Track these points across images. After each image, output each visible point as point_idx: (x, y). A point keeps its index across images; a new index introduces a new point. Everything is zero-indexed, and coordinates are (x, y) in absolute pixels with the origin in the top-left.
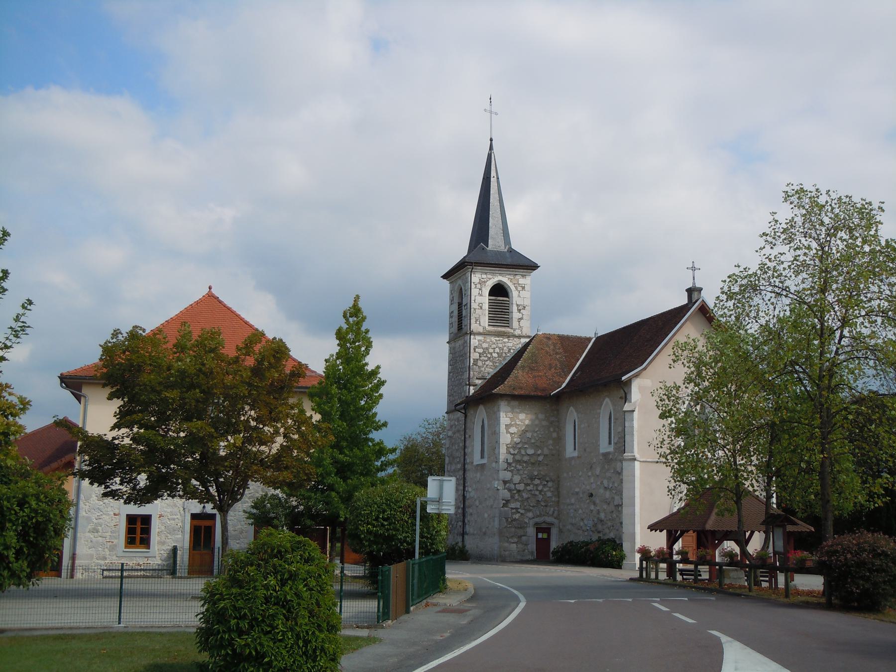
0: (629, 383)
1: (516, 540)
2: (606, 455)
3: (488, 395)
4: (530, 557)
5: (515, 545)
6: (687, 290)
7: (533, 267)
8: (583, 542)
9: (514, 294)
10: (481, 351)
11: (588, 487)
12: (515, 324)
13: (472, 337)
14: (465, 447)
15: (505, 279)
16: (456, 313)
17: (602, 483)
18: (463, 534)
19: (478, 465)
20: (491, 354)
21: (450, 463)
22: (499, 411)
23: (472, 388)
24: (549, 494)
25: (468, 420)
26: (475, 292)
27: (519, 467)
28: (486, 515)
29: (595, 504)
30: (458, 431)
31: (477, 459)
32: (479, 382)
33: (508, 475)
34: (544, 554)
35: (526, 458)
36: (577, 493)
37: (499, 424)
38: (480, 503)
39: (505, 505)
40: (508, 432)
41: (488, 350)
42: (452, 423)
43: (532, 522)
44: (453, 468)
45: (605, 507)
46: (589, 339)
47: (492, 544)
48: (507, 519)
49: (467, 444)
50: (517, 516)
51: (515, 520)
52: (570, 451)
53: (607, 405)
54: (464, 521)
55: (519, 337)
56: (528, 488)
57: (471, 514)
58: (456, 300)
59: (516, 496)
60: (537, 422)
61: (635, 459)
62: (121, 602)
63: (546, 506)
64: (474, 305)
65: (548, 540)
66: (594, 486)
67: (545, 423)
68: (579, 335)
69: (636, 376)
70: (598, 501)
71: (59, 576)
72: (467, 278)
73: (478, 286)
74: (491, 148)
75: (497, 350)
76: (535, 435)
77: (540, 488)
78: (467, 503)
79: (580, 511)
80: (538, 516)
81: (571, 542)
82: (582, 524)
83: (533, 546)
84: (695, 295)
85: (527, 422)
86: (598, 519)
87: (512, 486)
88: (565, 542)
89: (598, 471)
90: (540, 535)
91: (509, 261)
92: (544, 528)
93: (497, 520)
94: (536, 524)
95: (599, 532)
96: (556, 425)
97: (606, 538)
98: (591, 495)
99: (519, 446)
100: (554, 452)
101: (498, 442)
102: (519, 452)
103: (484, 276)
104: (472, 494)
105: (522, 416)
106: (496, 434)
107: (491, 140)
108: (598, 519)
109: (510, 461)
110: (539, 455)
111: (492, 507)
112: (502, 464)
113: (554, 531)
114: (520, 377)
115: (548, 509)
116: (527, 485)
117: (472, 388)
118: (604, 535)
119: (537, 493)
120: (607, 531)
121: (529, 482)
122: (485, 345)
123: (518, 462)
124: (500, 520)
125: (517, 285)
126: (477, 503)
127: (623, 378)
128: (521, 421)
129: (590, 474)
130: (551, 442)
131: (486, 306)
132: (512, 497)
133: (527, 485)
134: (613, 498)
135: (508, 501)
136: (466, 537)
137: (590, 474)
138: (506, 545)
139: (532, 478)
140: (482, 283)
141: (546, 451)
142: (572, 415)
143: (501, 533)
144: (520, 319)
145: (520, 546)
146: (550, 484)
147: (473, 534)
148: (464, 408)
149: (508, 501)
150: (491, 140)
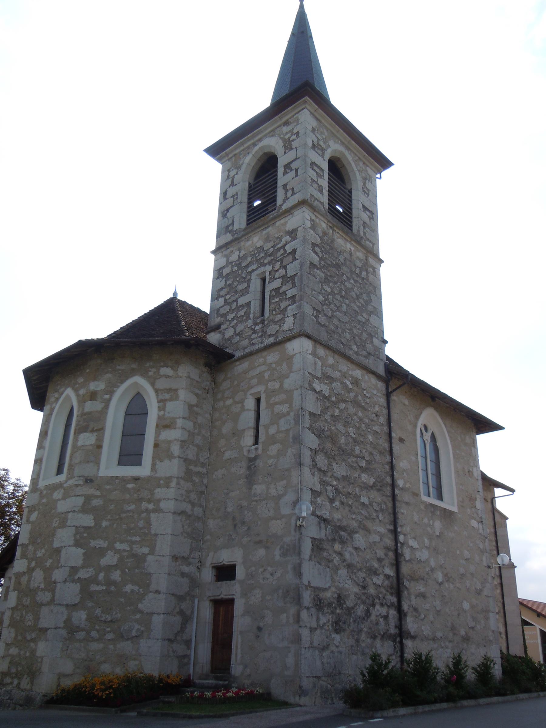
38: (448, 578)
57: (423, 596)
104: (424, 555)
111: (479, 592)
126: (440, 577)
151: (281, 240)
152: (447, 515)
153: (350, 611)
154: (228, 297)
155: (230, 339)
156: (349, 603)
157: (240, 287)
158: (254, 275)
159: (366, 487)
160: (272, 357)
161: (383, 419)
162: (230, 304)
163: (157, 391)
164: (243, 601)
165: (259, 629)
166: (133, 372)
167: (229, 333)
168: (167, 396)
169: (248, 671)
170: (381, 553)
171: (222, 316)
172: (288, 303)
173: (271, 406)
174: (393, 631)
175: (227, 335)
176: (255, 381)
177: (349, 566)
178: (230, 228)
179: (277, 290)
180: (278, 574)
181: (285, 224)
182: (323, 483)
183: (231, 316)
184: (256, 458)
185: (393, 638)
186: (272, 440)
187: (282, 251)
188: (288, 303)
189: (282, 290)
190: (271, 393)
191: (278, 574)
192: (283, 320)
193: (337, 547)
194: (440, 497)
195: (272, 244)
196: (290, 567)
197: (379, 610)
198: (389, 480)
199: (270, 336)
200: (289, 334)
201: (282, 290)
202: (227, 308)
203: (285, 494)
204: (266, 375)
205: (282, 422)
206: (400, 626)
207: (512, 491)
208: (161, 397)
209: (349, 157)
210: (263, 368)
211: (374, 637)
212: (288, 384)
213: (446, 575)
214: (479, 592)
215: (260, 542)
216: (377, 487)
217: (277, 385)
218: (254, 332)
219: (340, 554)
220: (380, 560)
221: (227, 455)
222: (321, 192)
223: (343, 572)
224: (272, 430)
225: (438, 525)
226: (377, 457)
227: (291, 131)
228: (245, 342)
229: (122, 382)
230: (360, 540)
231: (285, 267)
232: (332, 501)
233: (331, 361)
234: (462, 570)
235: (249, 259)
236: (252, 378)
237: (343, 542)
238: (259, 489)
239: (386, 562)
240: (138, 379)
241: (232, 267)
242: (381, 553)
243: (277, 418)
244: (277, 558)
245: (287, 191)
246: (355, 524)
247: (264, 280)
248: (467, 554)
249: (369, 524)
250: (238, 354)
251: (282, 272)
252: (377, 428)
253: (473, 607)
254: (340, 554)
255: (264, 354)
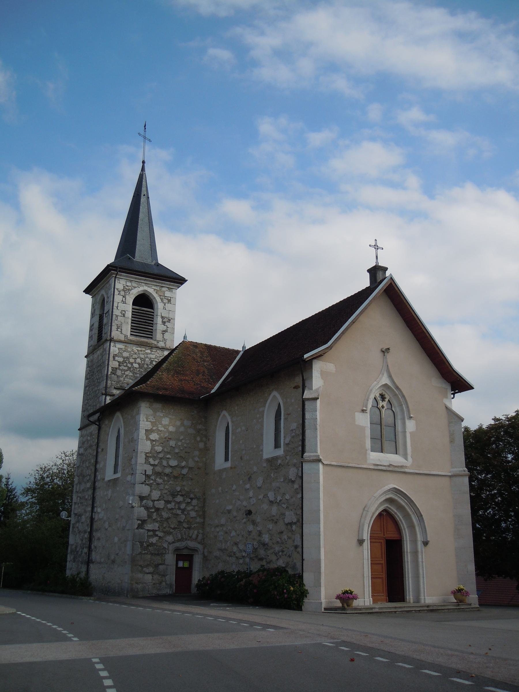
0: (308, 365)
1: (151, 569)
2: (271, 461)
3: (128, 400)
4: (168, 591)
5: (149, 577)
6: (369, 271)
7: (180, 281)
8: (239, 572)
9: (159, 305)
10: (121, 359)
11: (245, 503)
12: (159, 336)
13: (112, 344)
14: (96, 462)
15: (150, 288)
16: (96, 325)
17: (266, 496)
18: (89, 562)
19: (109, 481)
20: (132, 364)
21: (79, 483)
22: (138, 413)
23: (108, 398)
24: (193, 514)
25: (102, 433)
26: (118, 298)
27: (159, 480)
28: (116, 540)
29: (254, 523)
30: (91, 446)
31: (109, 475)
32: (117, 392)
33: (145, 490)
34: (185, 590)
35: (168, 471)
36: (229, 511)
37: (137, 429)
39: (140, 526)
40: (148, 439)
41: (129, 358)
42: (84, 439)
43: (172, 548)
44: (82, 488)
45: (270, 526)
46: (238, 352)
47: (120, 575)
48: (141, 543)
49: (99, 459)
50: (154, 540)
51: (152, 544)
52: (220, 462)
53: (275, 398)
54: (90, 548)
55: (163, 349)
56: (169, 506)
57: (99, 539)
58: (98, 312)
59: (155, 516)
60: (182, 429)
61: (319, 461)
63: (189, 528)
64: (116, 312)
65: (189, 570)
66: (253, 501)
67: (191, 431)
68: (227, 347)
69: (318, 357)
70: (258, 520)
72: (110, 285)
73: (122, 293)
74: (143, 169)
75: (138, 360)
76: (180, 444)
77: (183, 506)
78: (95, 527)
79: (233, 533)
80: (179, 540)
81: (222, 572)
82: (235, 549)
83: (171, 578)
84: (380, 276)
85: (171, 429)
86: (259, 542)
87: (150, 504)
88: (214, 572)
89: (260, 482)
90: (181, 564)
91: (156, 271)
92: (185, 556)
93: (129, 544)
94: (177, 549)
95: (261, 559)
96: (205, 435)
97: (273, 566)
98: (249, 513)
99: (161, 455)
100: (201, 465)
101: (135, 450)
102: (160, 463)
103: (129, 284)
104: (101, 516)
105: (166, 421)
106: (133, 441)
107: (144, 162)
108: (259, 542)
109: (149, 472)
110: (183, 467)
112: (140, 477)
113: (197, 559)
114: (164, 377)
115: (191, 532)
116: (168, 502)
117: (108, 398)
118: (269, 562)
119: (179, 512)
120: (274, 558)
121: (170, 498)
122: (126, 354)
123: (158, 474)
124: (133, 545)
125: (163, 297)
126: (106, 525)
127: (306, 356)
128: (164, 426)
129: (248, 486)
130: (197, 453)
131: (129, 314)
132: (149, 516)
133: (168, 502)
134: (284, 514)
135: (144, 522)
136: (91, 565)
137: (248, 486)
138: (140, 575)
139: (174, 495)
140: (127, 290)
141: (191, 464)
142: (224, 419)
143: (133, 560)
144: (164, 332)
145: (156, 577)
146: (195, 502)
147: (100, 563)
148: (99, 420)
149: (144, 522)
150: (144, 162)
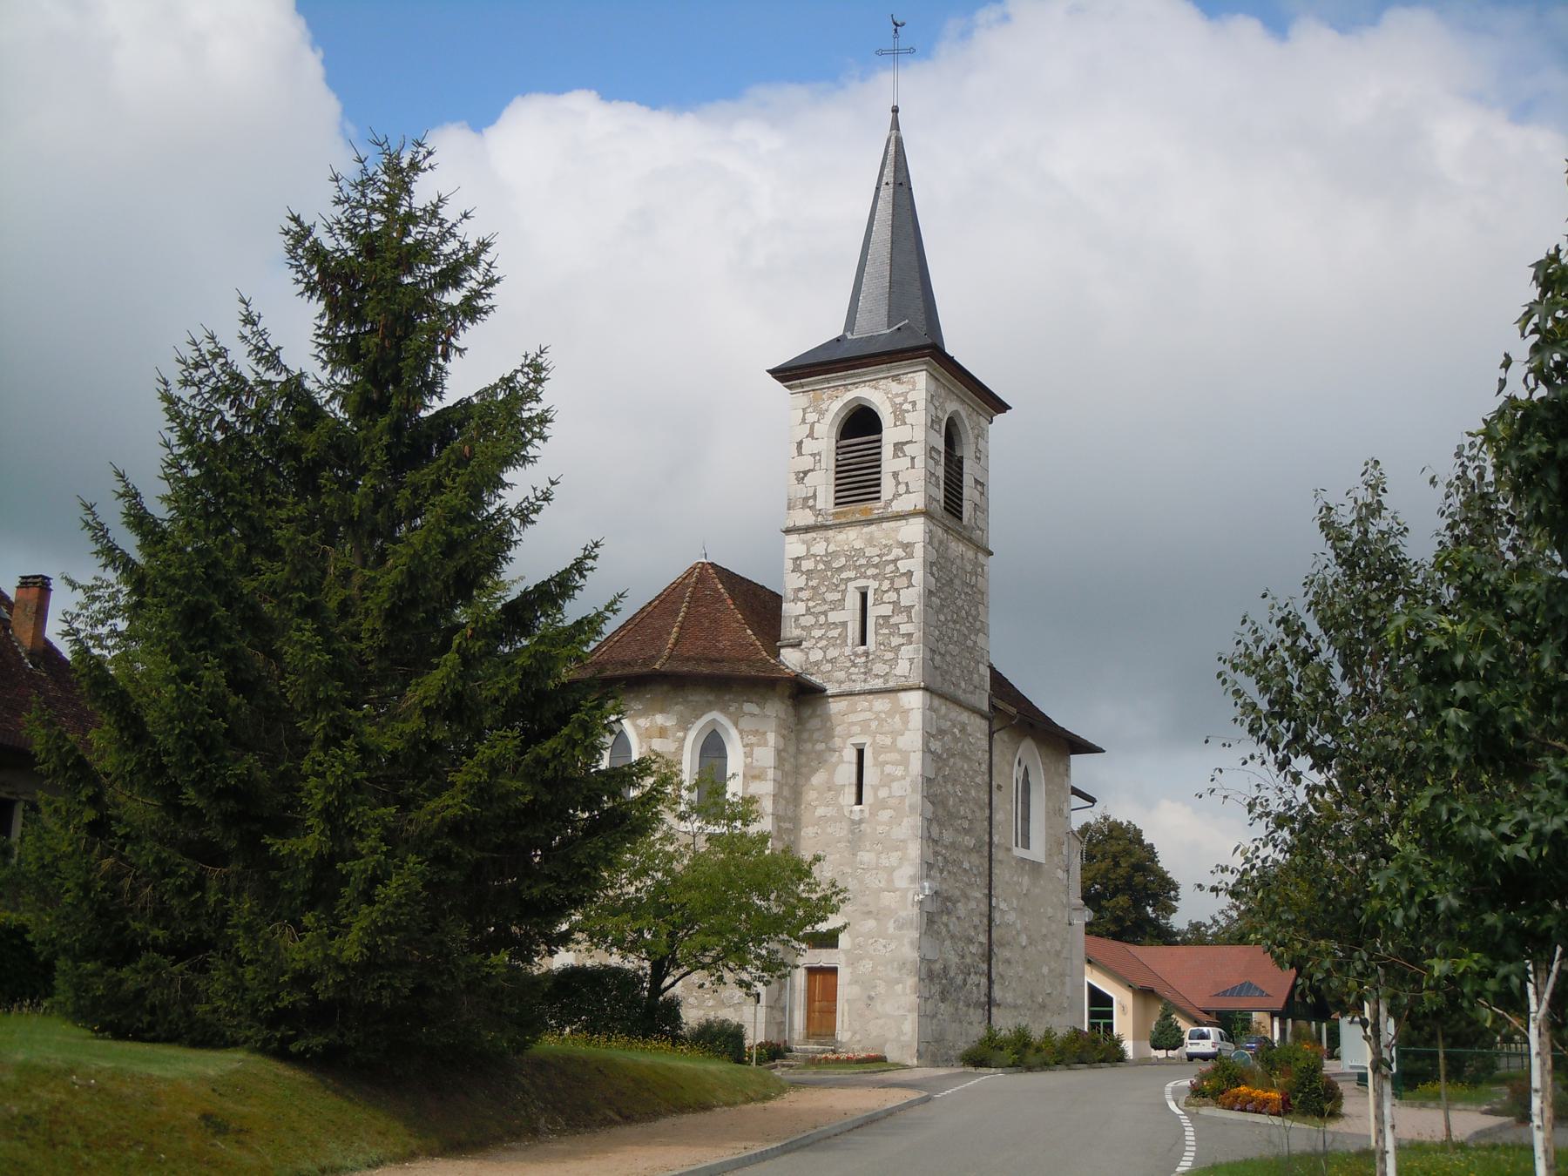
28: (1045, 970)
38: (1031, 942)
57: (1008, 962)
62: (1448, 1128)
71: (833, 971)
74: (895, 125)
104: (1011, 917)
107: (895, 110)
111: (1058, 954)
126: (1024, 940)
136: (994, 1010)
147: (1015, 1007)
150: (895, 110)
151: (890, 551)
152: (1035, 867)
153: (952, 980)
154: (811, 604)
155: (816, 663)
156: (952, 974)
157: (831, 596)
158: (851, 586)
159: (969, 851)
160: (881, 704)
161: (984, 767)
162: (816, 615)
163: (741, 732)
164: (849, 970)
165: (870, 998)
166: (710, 706)
167: (816, 655)
168: (753, 739)
169: (858, 1037)
170: (976, 920)
171: (803, 628)
172: (901, 641)
173: (877, 764)
174: (983, 999)
175: (813, 658)
176: (856, 729)
177: (952, 937)
178: (811, 503)
179: (886, 618)
180: (893, 946)
181: (897, 530)
182: (936, 854)
183: (817, 633)
184: (861, 821)
185: (981, 1006)
186: (882, 805)
187: (891, 567)
188: (901, 641)
189: (892, 621)
190: (879, 750)
191: (893, 946)
192: (896, 659)
193: (945, 918)
194: (1026, 845)
195: (876, 551)
196: (906, 941)
197: (973, 979)
198: (986, 838)
199: (877, 676)
200: (902, 682)
201: (892, 621)
202: (810, 620)
203: (900, 866)
204: (874, 725)
205: (895, 785)
206: (989, 995)
207: (1092, 800)
208: (746, 740)
209: (963, 414)
210: (868, 715)
211: (968, 1006)
212: (902, 742)
213: (1029, 937)
214: (1058, 954)
215: (870, 912)
216: (976, 849)
217: (888, 741)
218: (854, 665)
219: (946, 925)
220: (975, 927)
221: (820, 811)
222: (938, 486)
223: (948, 943)
224: (883, 793)
225: (1026, 880)
226: (978, 814)
227: (904, 394)
228: (841, 675)
229: (697, 718)
230: (961, 909)
231: (897, 590)
232: (941, 872)
233: (943, 710)
234: (1044, 931)
235: (843, 561)
236: (853, 724)
237: (949, 913)
238: (866, 857)
239: (981, 929)
240: (715, 715)
241: (817, 562)
242: (976, 920)
243: (888, 780)
244: (891, 930)
245: (898, 483)
246: (958, 893)
247: (864, 597)
248: (1050, 911)
249: (969, 892)
250: (831, 689)
251: (892, 596)
252: (978, 780)
253: (1051, 971)
254: (946, 925)
255: (871, 697)
